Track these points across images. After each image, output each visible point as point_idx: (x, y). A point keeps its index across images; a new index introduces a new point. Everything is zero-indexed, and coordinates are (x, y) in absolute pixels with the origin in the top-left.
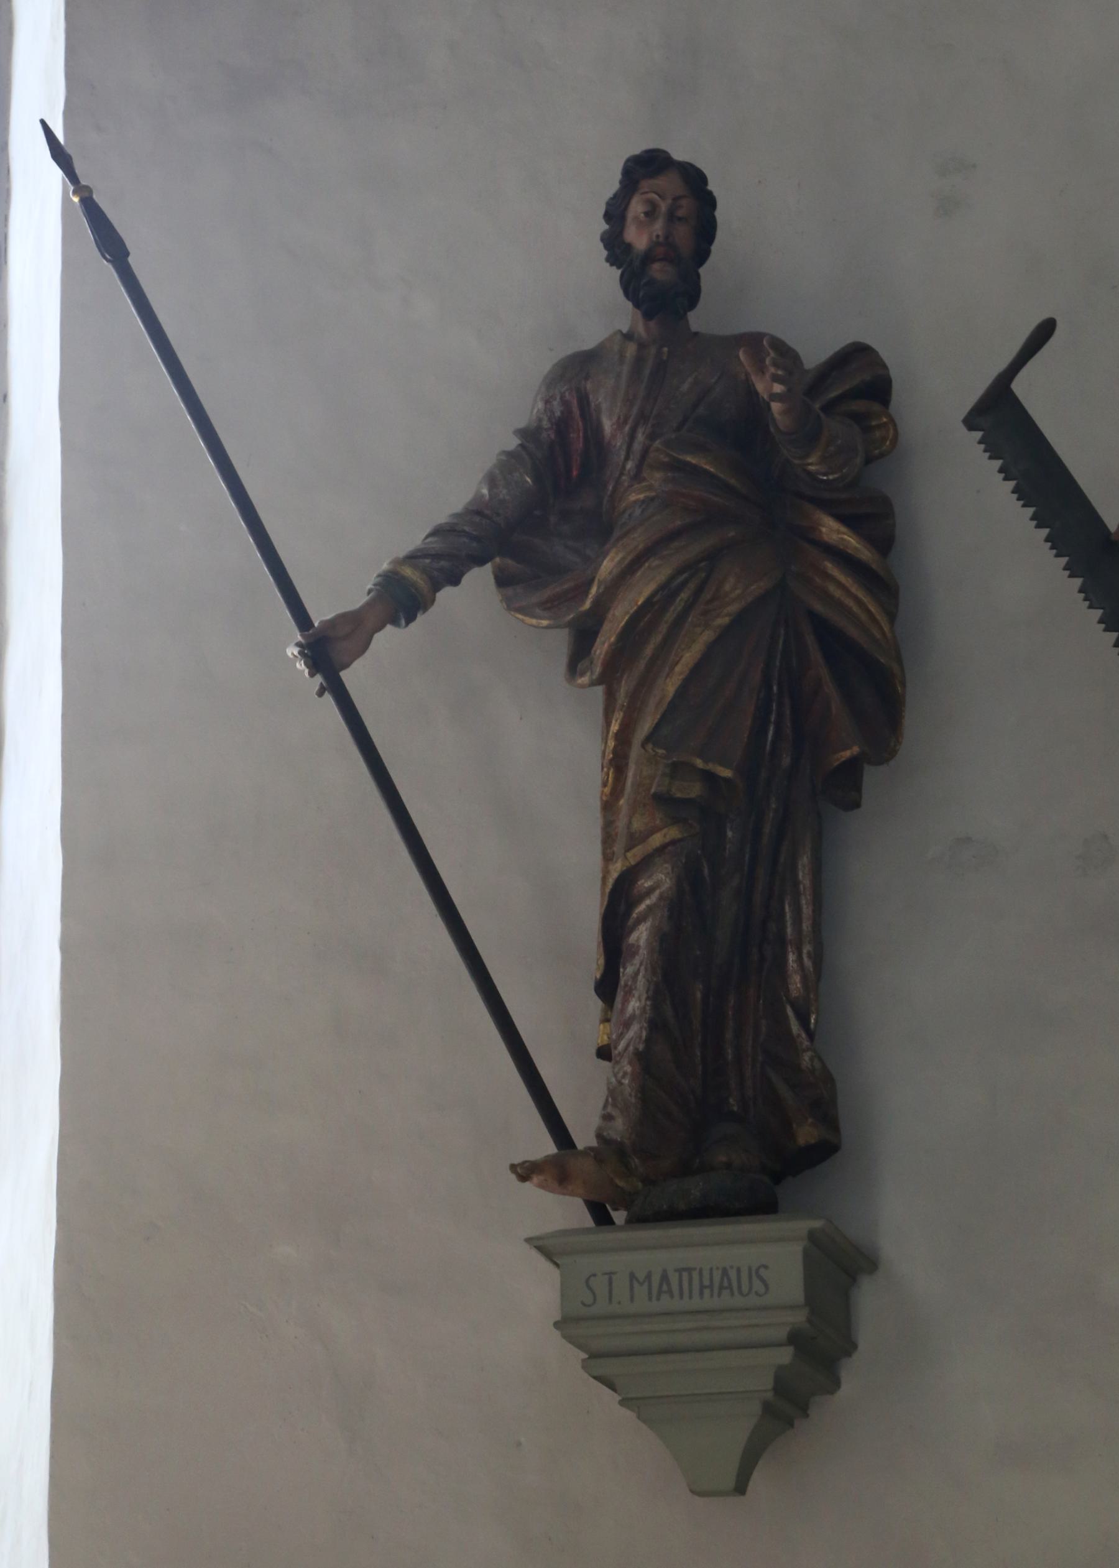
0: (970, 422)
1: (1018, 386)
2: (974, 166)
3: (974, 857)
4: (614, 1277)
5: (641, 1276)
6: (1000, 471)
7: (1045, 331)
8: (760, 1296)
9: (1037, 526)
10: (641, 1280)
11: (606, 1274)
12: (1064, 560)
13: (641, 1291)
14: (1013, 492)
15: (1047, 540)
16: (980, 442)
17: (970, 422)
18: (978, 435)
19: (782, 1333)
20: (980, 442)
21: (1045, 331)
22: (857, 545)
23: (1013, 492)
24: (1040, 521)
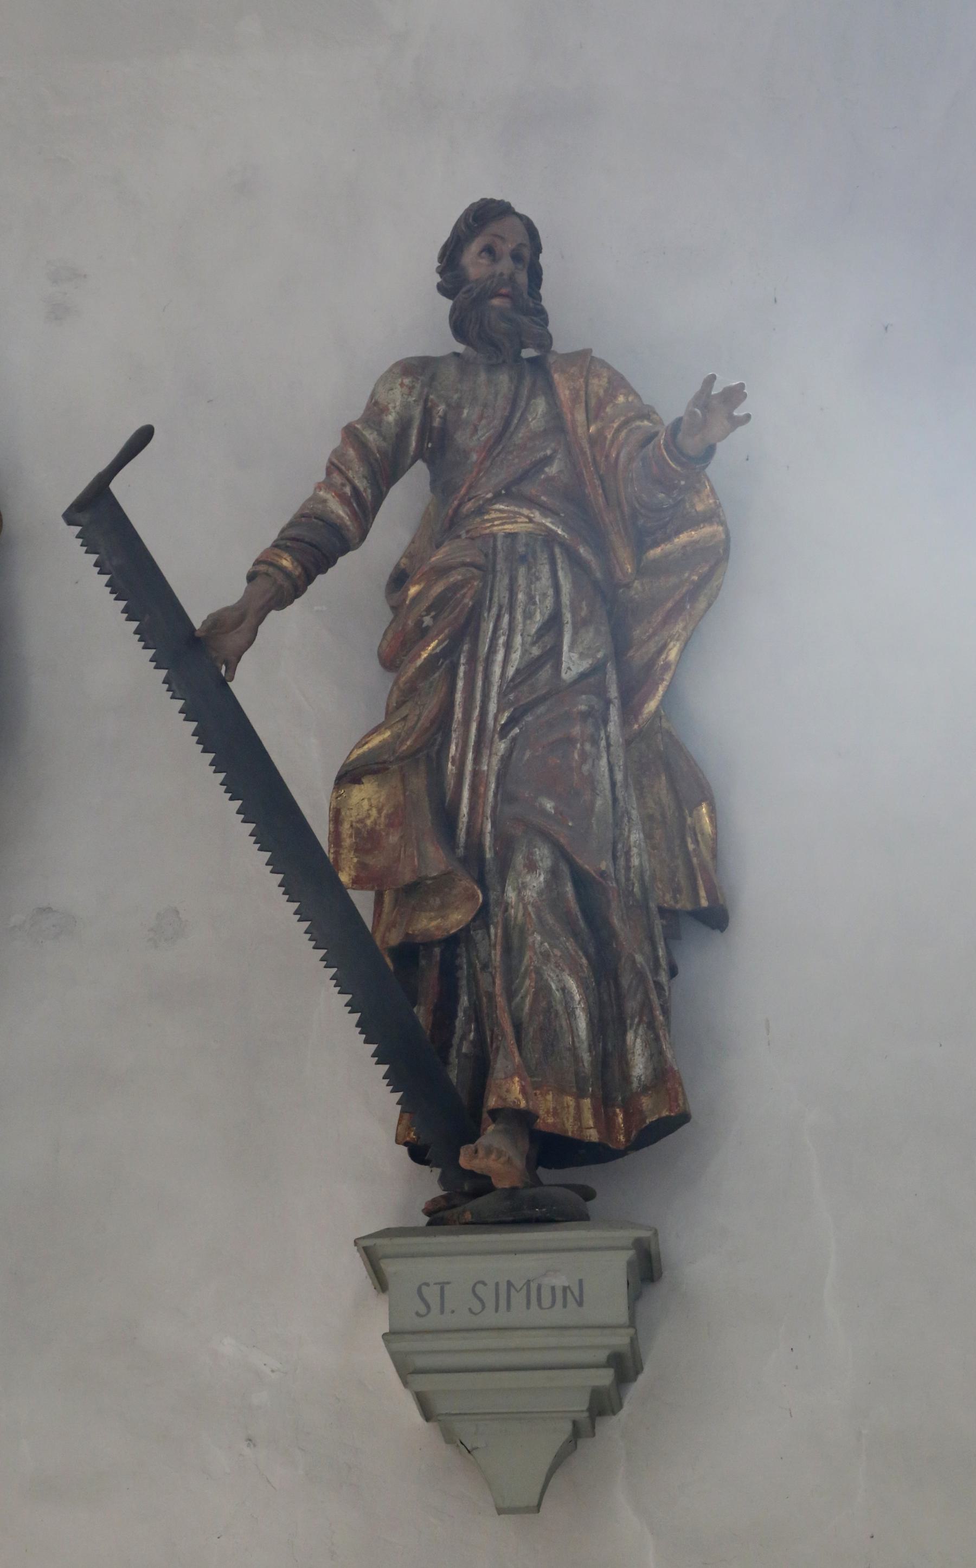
0: (70, 517)
1: (116, 486)
2: (85, 276)
3: (54, 926)
4: (447, 1287)
5: (519, 1284)
6: (96, 565)
7: (143, 437)
8: (475, 1314)
9: (128, 619)
10: (518, 1288)
11: (439, 1284)
12: (151, 652)
13: (518, 1299)
14: (107, 585)
15: (136, 632)
16: (78, 537)
17: (70, 517)
18: (77, 529)
19: (602, 1356)
20: (78, 537)
21: (143, 437)
22: (349, 523)
23: (107, 585)
24: (130, 613)
